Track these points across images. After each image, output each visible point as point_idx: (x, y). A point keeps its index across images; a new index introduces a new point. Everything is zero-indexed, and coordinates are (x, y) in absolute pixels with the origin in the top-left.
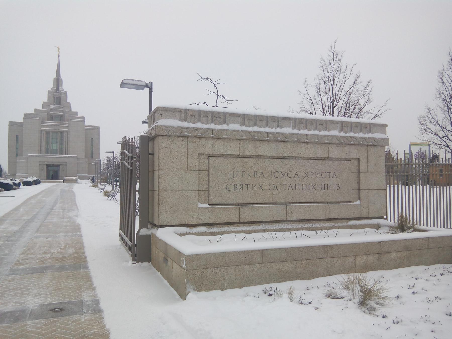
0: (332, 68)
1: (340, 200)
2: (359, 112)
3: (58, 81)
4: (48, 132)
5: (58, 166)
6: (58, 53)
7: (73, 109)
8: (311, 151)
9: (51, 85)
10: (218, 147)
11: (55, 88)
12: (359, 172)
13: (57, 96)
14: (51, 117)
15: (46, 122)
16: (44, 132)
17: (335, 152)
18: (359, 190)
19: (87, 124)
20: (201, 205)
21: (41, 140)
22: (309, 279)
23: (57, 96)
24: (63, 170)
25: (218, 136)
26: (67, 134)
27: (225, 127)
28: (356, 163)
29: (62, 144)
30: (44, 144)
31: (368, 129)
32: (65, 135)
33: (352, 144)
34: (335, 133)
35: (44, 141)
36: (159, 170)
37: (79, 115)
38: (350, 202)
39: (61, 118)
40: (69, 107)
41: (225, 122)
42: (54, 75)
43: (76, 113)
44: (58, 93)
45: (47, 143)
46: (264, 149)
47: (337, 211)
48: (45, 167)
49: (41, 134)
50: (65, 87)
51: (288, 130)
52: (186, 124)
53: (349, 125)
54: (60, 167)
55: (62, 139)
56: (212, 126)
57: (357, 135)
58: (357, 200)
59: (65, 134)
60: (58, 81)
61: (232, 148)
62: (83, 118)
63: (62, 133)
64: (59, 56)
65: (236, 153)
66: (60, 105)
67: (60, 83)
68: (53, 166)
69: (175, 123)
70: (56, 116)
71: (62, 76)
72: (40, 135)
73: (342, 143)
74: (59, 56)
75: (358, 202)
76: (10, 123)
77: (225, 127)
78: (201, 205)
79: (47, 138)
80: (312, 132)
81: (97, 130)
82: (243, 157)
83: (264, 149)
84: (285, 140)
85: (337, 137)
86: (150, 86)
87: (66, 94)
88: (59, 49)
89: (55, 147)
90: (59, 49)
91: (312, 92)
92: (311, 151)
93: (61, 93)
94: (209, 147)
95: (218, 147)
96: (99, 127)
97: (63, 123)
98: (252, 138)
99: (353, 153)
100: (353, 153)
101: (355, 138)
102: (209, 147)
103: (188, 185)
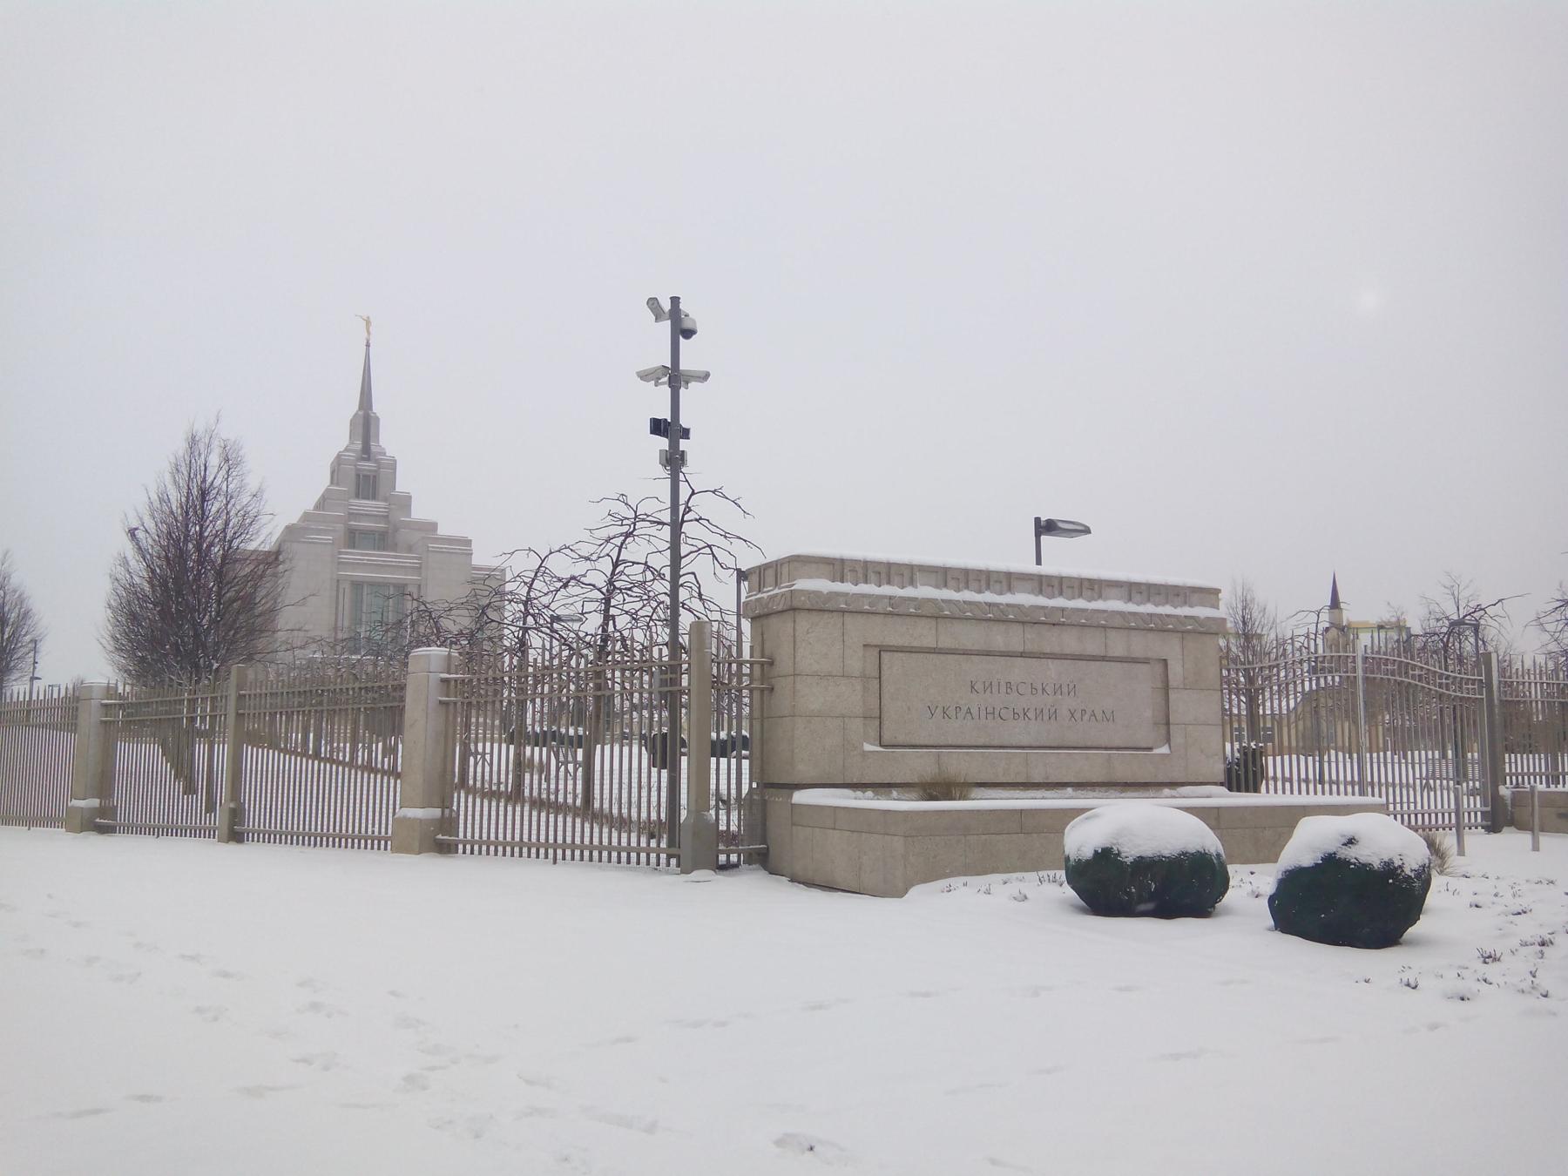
1: (981, 742)
2: (628, 535)
3: (365, 425)
4: (357, 585)
7: (419, 512)
9: (339, 438)
10: (896, 633)
11: (358, 445)
14: (354, 538)
15: (353, 555)
16: (347, 586)
18: (1168, 724)
20: (868, 747)
22: (894, 889)
28: (1159, 668)
31: (906, 578)
33: (1151, 630)
38: (1150, 749)
39: (383, 539)
40: (405, 502)
42: (353, 406)
43: (433, 526)
44: (368, 459)
47: (1124, 768)
50: (388, 441)
51: (924, 591)
53: (1056, 584)
60: (365, 425)
62: (468, 542)
64: (368, 345)
66: (374, 498)
70: (367, 533)
71: (377, 408)
74: (368, 345)
75: (1164, 750)
78: (868, 747)
84: (935, 614)
85: (1121, 614)
87: (393, 465)
88: (368, 322)
90: (368, 322)
93: (377, 461)
95: (896, 633)
97: (408, 560)
101: (997, 605)
103: (245, 666)
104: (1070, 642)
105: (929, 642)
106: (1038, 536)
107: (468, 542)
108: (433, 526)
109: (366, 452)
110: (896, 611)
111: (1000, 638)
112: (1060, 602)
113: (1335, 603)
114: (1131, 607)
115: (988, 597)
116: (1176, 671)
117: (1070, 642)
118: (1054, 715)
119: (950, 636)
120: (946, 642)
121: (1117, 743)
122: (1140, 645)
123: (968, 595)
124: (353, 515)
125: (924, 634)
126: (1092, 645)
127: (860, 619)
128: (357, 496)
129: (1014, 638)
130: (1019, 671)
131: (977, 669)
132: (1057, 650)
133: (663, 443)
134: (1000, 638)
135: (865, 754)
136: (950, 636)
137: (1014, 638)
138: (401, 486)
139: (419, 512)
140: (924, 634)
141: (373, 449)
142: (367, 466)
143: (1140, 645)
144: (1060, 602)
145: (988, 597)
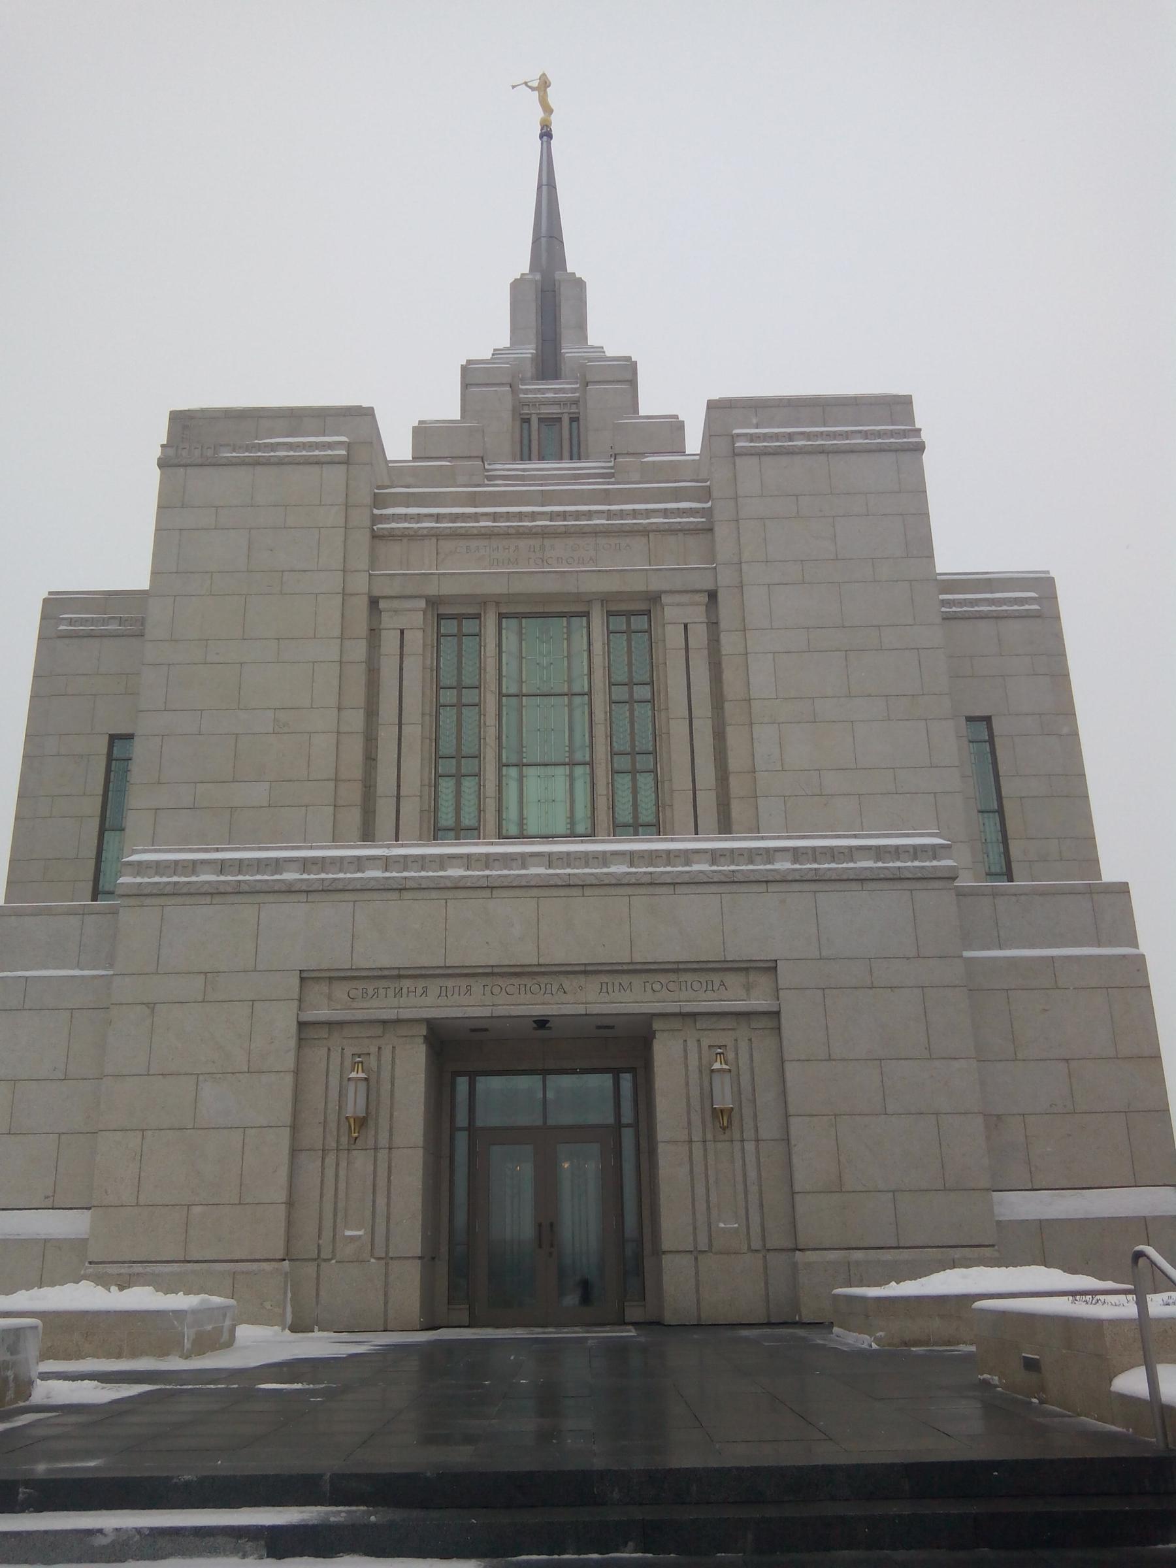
4: (452, 617)
5: (624, 1050)
6: (540, 114)
13: (549, 298)
16: (408, 621)
21: (371, 712)
23: (549, 298)
24: (722, 1119)
26: (697, 615)
30: (414, 768)
32: (674, 636)
35: (414, 731)
36: (375, 1149)
42: (518, 261)
48: (409, 1070)
49: (374, 633)
54: (670, 1056)
55: (638, 690)
58: (482, 1129)
59: (679, 616)
63: (635, 613)
64: (546, 134)
66: (576, 454)
67: (566, 314)
68: (542, 1046)
72: (358, 650)
74: (546, 134)
79: (452, 694)
86: (988, 720)
128: (525, 454)
142: (549, 390)
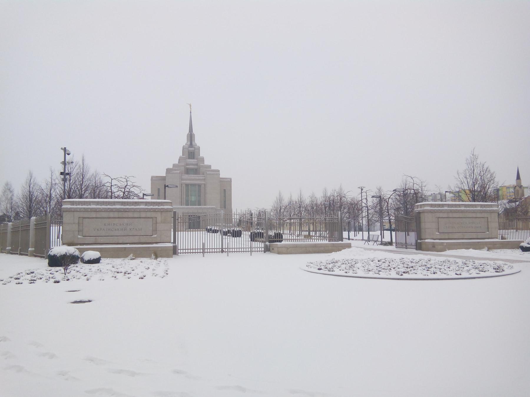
0: (472, 162)
3: (191, 137)
4: (187, 185)
7: (206, 163)
8: (470, 215)
9: (184, 141)
10: (441, 215)
11: (189, 143)
12: (488, 222)
13: (191, 151)
14: (188, 171)
15: (186, 176)
16: (184, 186)
17: (479, 215)
19: (221, 176)
20: (79, 237)
23: (191, 151)
25: (441, 212)
27: (443, 208)
29: (199, 196)
34: (479, 208)
37: (213, 168)
39: (196, 171)
40: (203, 160)
41: (443, 207)
42: (187, 131)
43: (210, 167)
45: (187, 195)
46: (455, 215)
50: (198, 141)
51: (463, 208)
52: (146, 207)
55: (199, 191)
56: (439, 208)
57: (160, 207)
59: (203, 186)
60: (191, 137)
61: (445, 215)
62: (219, 171)
63: (199, 186)
65: (446, 216)
66: (194, 159)
69: (429, 208)
70: (192, 169)
71: (194, 131)
73: (145, 210)
76: (152, 177)
77: (443, 208)
78: (79, 237)
79: (187, 191)
80: (471, 209)
81: (228, 182)
82: (140, 218)
83: (455, 215)
84: (462, 212)
87: (199, 148)
88: (190, 106)
89: (193, 199)
90: (190, 106)
91: (462, 176)
92: (470, 215)
93: (194, 148)
94: (439, 215)
95: (441, 215)
96: (231, 179)
97: (201, 177)
98: (451, 211)
99: (486, 215)
100: (486, 215)
102: (439, 215)
104: (130, 215)
105: (94, 216)
106: (165, 188)
107: (219, 171)
108: (210, 166)
109: (191, 144)
110: (86, 210)
111: (112, 215)
112: (128, 207)
113: (518, 177)
114: (146, 207)
115: (109, 207)
116: (159, 219)
117: (130, 215)
118: (125, 229)
119: (99, 215)
120: (98, 216)
121: (142, 234)
122: (149, 215)
123: (103, 207)
124: (187, 164)
125: (94, 215)
126: (136, 215)
127: (78, 213)
128: (189, 159)
129: (116, 215)
130: (117, 221)
131: (107, 221)
132: (127, 216)
133: (62, 177)
134: (112, 215)
135: (78, 238)
136: (99, 215)
137: (116, 215)
138: (202, 155)
139: (206, 163)
140: (94, 215)
141: (193, 144)
143: (149, 215)
144: (128, 207)
145: (109, 207)
